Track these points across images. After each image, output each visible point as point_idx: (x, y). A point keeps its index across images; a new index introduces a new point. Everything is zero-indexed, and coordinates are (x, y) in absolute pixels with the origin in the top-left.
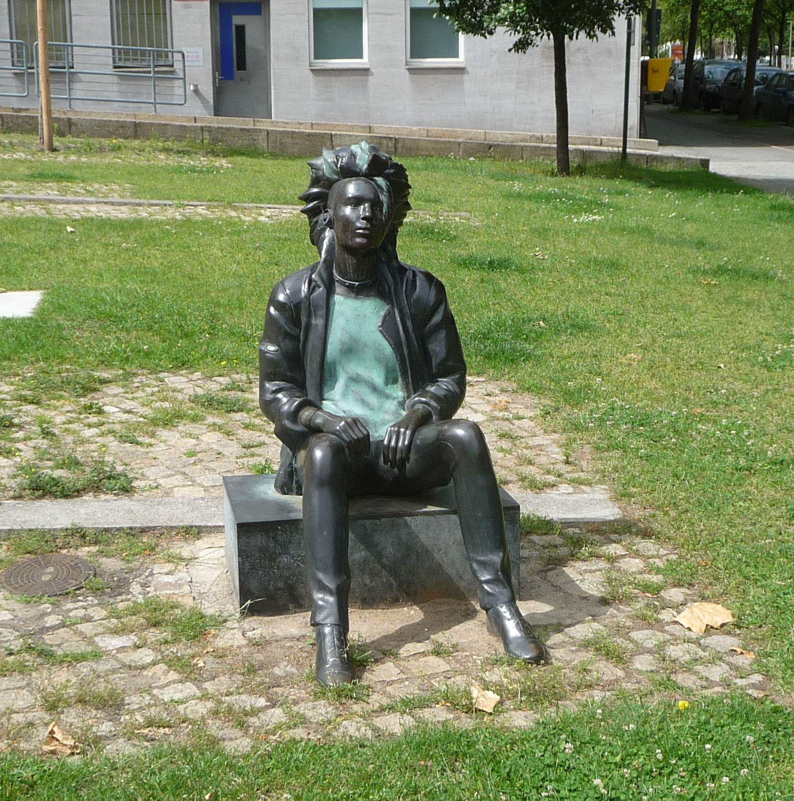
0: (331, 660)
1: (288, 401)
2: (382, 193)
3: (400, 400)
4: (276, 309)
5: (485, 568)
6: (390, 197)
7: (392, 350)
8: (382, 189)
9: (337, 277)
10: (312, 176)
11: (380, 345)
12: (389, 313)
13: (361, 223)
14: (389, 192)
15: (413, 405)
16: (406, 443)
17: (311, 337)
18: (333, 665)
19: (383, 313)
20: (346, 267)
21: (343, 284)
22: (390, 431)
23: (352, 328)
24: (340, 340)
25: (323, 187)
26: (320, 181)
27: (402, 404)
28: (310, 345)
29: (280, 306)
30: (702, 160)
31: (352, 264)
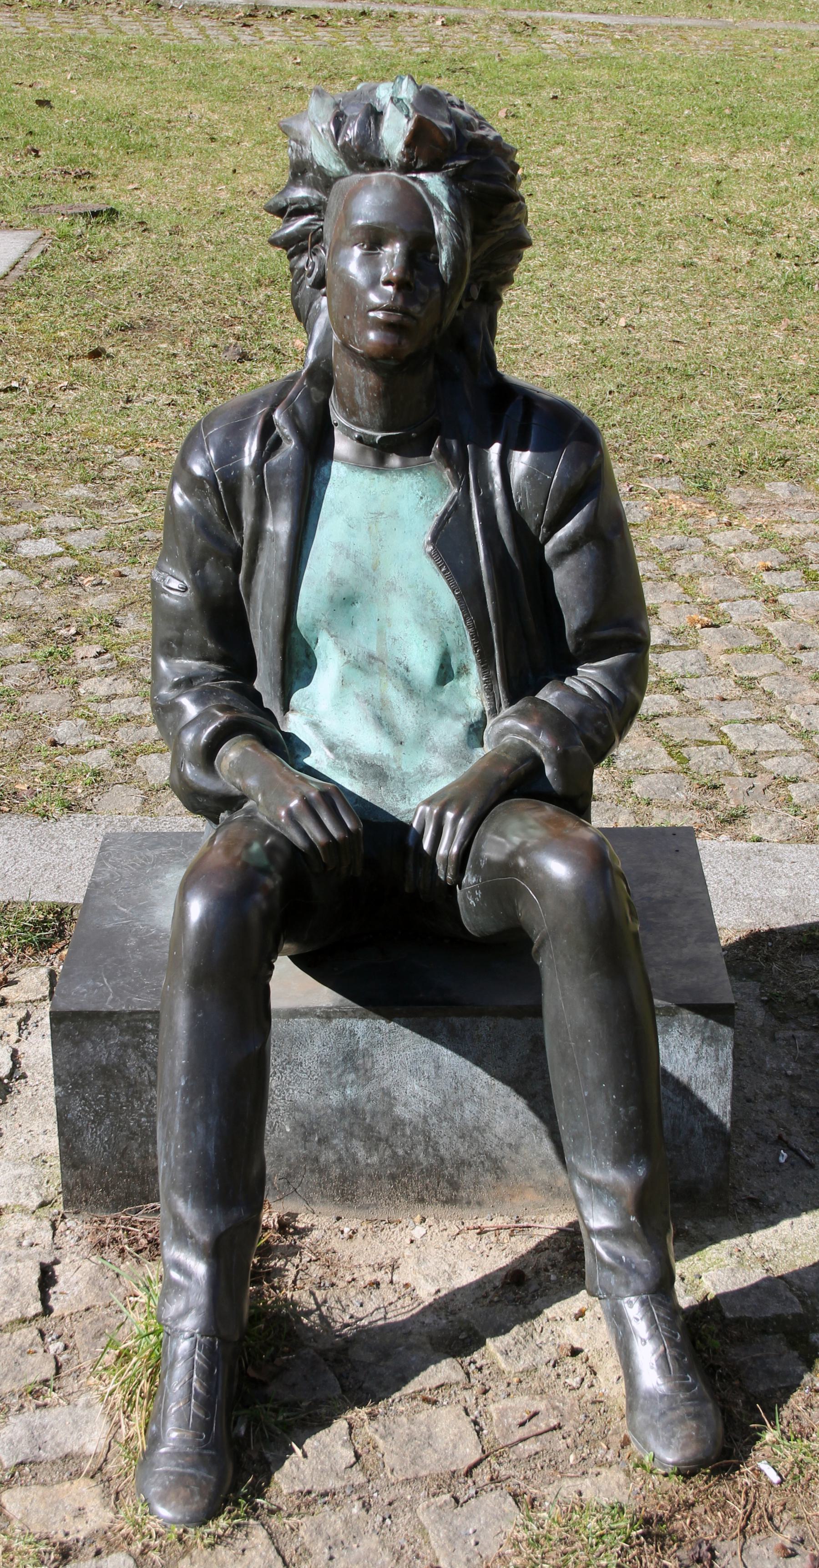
0: (174, 1435)
1: (199, 716)
2: (440, 219)
3: (474, 719)
4: (187, 490)
5: (600, 1199)
6: (458, 225)
7: (455, 602)
8: (440, 206)
9: (336, 416)
10: (290, 157)
11: (427, 588)
12: (456, 507)
13: (381, 295)
14: (456, 210)
15: (501, 735)
16: (455, 849)
17: (263, 562)
18: (170, 1455)
19: (439, 508)
20: (352, 393)
21: (348, 433)
22: (423, 813)
23: (362, 543)
24: (331, 574)
25: (314, 185)
26: (304, 172)
27: (476, 731)
28: (260, 577)
29: (194, 485)
30: (52, 1021)
31: (368, 389)
